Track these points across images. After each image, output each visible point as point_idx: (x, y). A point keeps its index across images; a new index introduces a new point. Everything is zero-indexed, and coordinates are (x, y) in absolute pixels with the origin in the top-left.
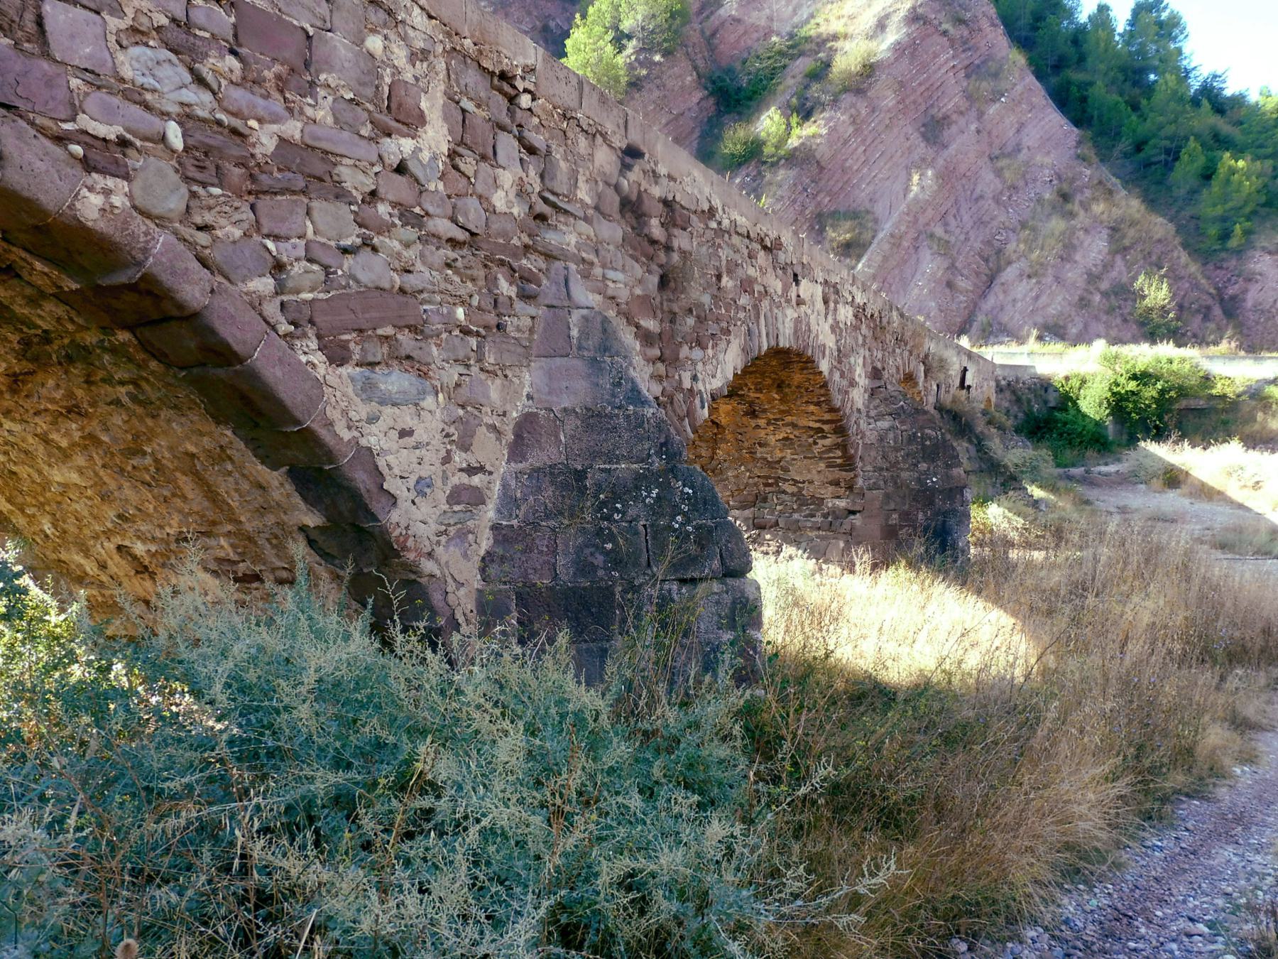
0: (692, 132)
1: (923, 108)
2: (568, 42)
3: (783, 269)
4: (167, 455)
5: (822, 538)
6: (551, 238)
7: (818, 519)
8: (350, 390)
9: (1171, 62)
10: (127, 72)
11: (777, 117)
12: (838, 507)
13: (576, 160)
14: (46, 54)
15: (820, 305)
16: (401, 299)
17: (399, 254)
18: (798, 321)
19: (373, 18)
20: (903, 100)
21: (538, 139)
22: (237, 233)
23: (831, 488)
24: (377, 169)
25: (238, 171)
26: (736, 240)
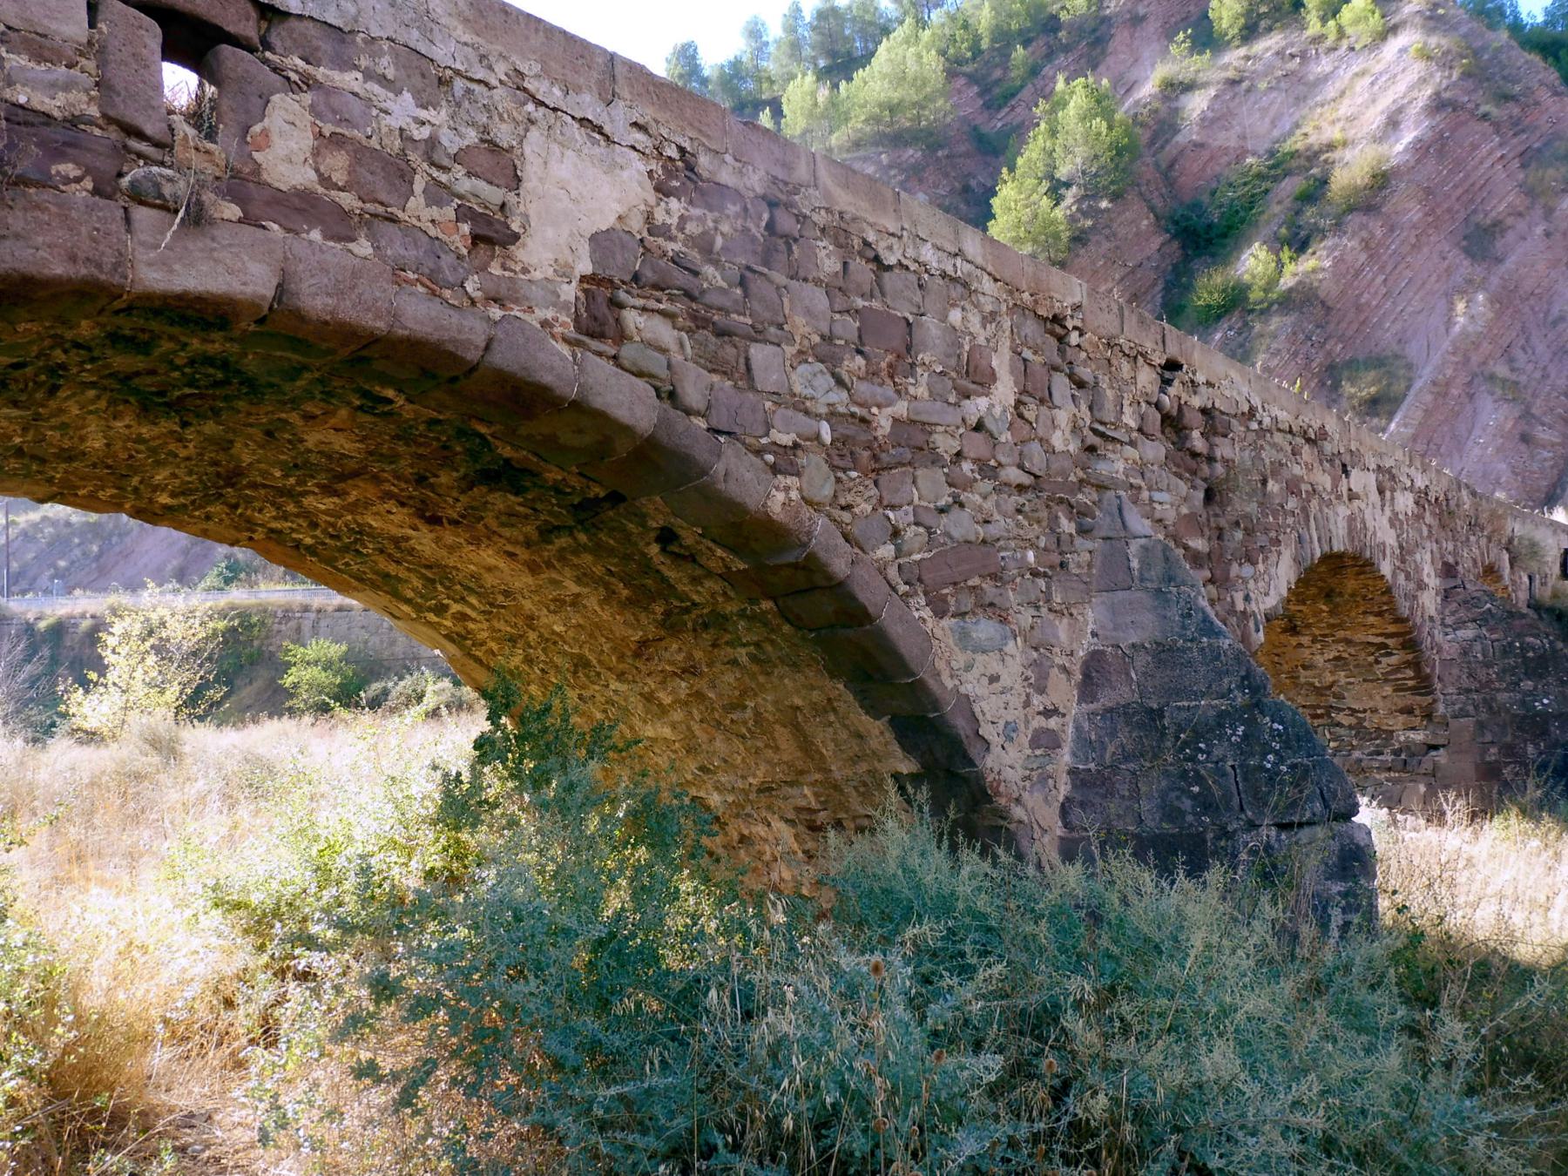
0: (1154, 285)
1: (1462, 215)
2: (996, 202)
3: (1331, 461)
4: (770, 708)
5: (1395, 781)
6: (1102, 468)
7: (1388, 757)
8: (951, 642)
10: (798, 389)
11: (1263, 255)
12: (1413, 742)
13: (1120, 386)
14: (753, 388)
15: (1374, 497)
16: (984, 549)
17: (980, 507)
18: (1351, 519)
19: (954, 294)
20: (1433, 210)
21: (1085, 373)
22: (869, 508)
23: (1402, 718)
24: (962, 430)
25: (866, 454)
26: (1278, 438)
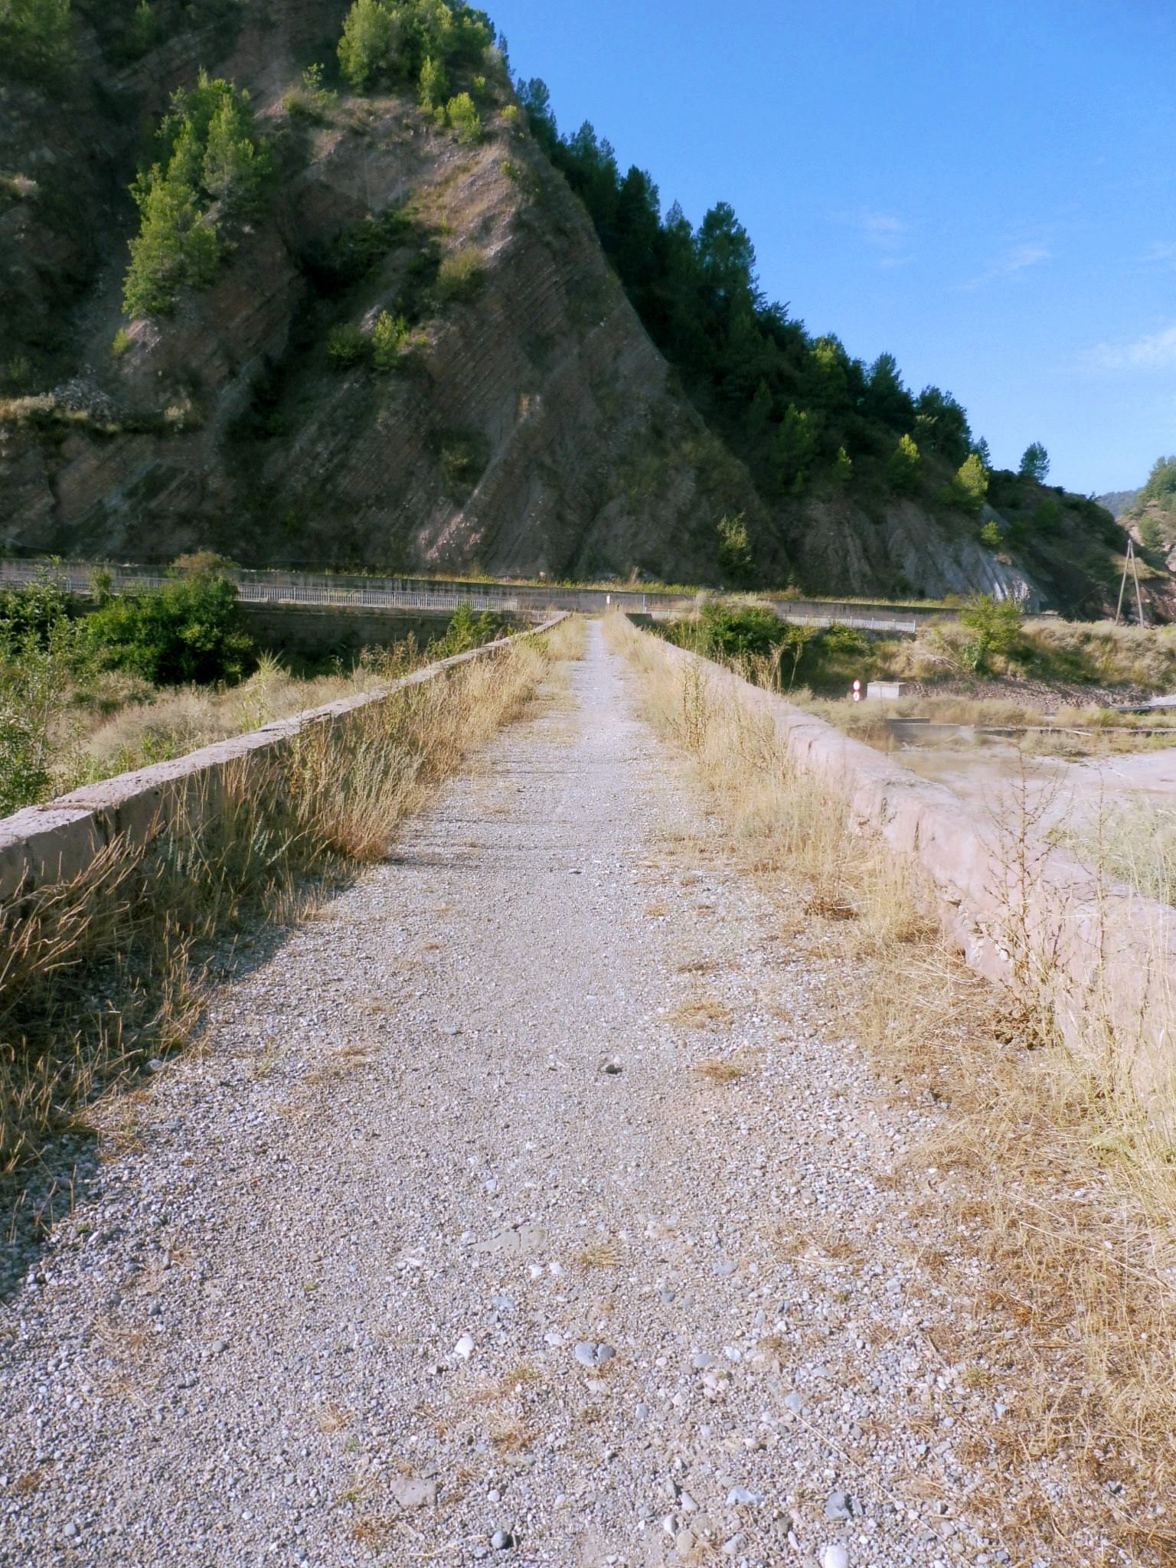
9: (739, 276)
